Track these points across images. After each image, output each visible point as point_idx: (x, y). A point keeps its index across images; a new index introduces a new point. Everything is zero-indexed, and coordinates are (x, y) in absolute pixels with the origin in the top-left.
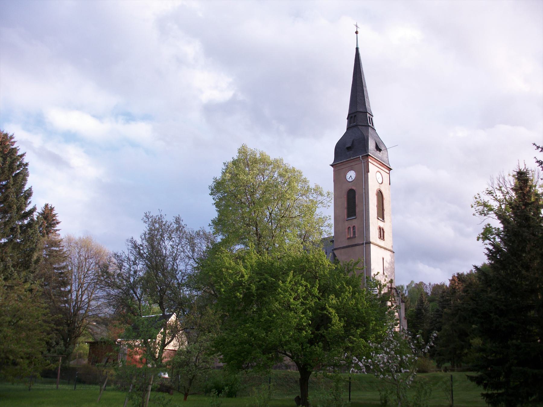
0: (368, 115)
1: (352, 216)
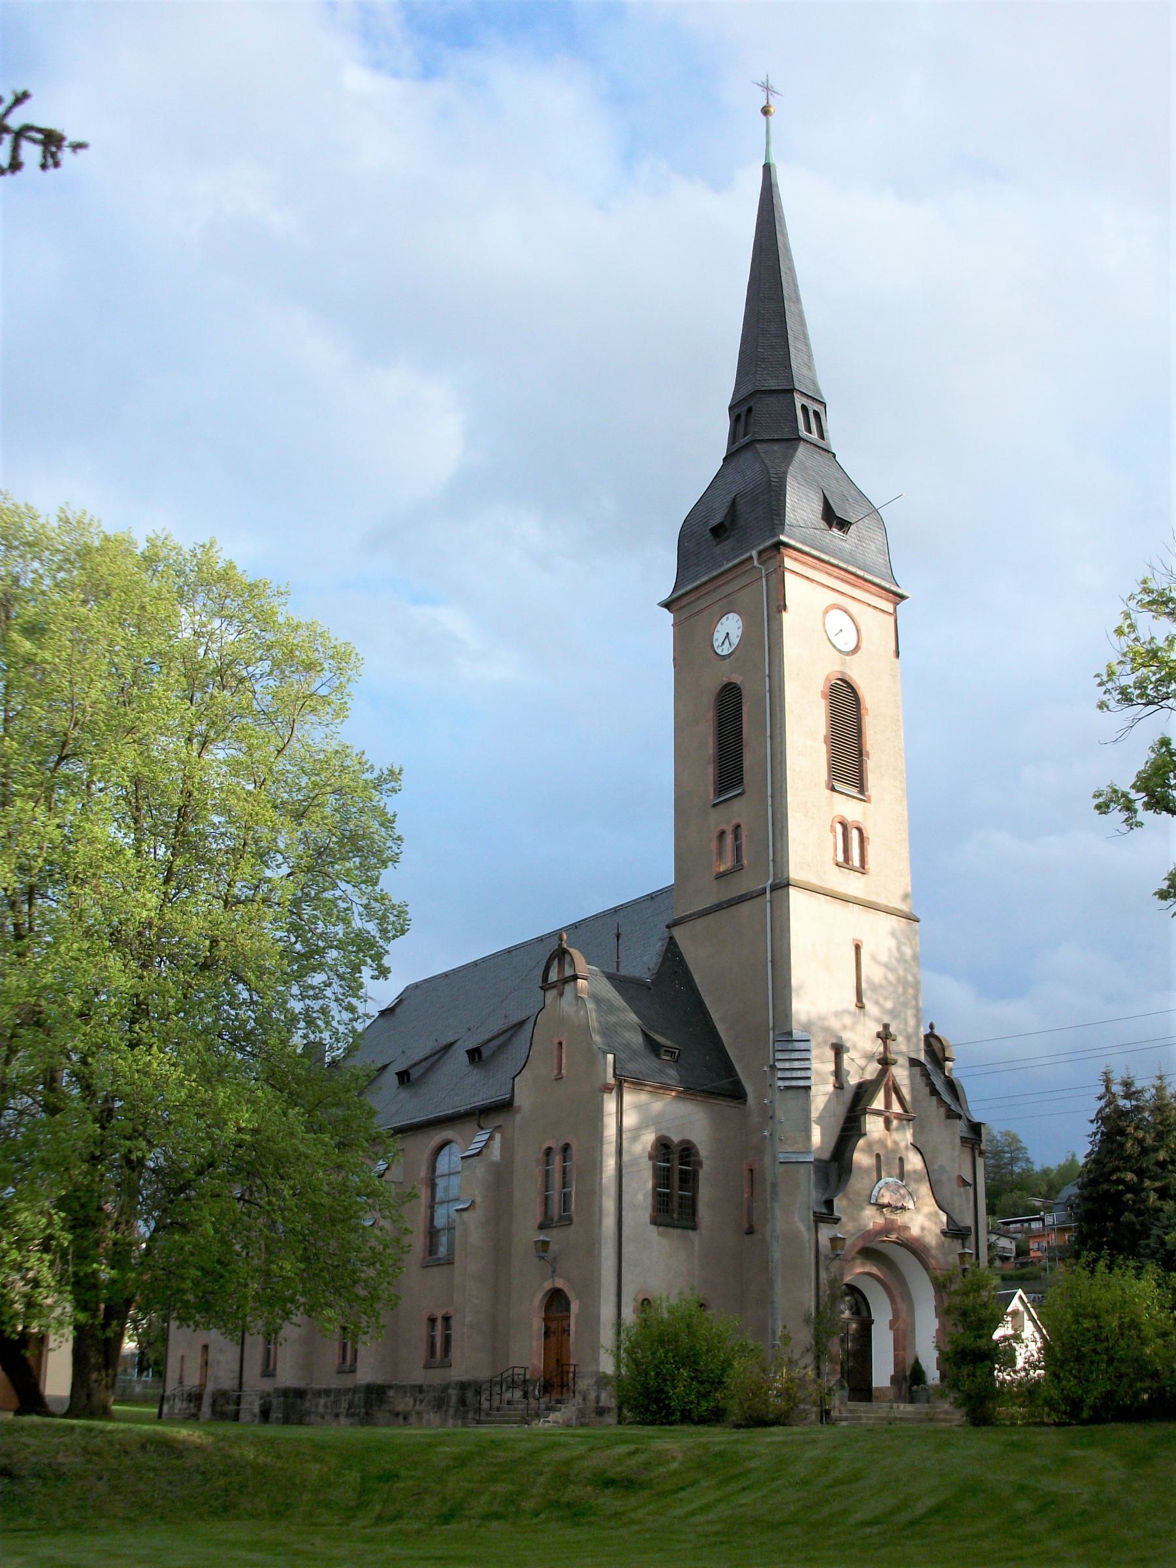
0: (799, 401)
1: (730, 787)
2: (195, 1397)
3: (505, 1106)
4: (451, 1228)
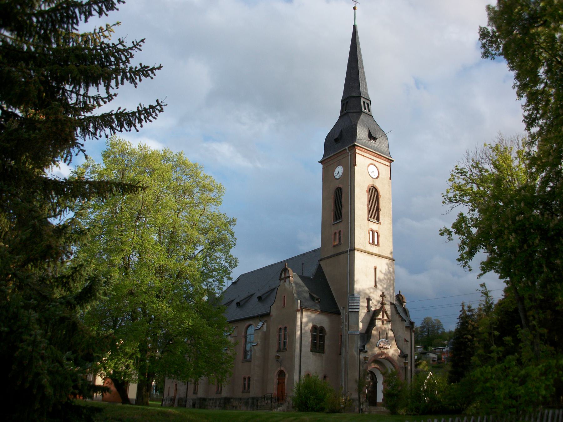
0: (362, 100)
2: (173, 400)
3: (268, 315)
4: (251, 351)
